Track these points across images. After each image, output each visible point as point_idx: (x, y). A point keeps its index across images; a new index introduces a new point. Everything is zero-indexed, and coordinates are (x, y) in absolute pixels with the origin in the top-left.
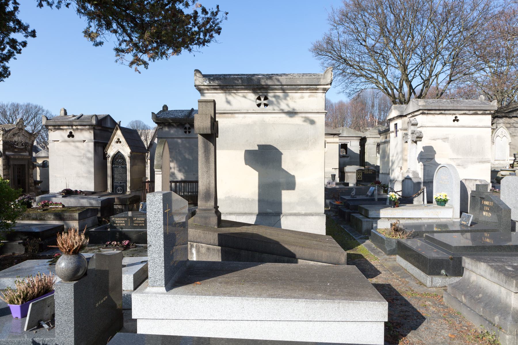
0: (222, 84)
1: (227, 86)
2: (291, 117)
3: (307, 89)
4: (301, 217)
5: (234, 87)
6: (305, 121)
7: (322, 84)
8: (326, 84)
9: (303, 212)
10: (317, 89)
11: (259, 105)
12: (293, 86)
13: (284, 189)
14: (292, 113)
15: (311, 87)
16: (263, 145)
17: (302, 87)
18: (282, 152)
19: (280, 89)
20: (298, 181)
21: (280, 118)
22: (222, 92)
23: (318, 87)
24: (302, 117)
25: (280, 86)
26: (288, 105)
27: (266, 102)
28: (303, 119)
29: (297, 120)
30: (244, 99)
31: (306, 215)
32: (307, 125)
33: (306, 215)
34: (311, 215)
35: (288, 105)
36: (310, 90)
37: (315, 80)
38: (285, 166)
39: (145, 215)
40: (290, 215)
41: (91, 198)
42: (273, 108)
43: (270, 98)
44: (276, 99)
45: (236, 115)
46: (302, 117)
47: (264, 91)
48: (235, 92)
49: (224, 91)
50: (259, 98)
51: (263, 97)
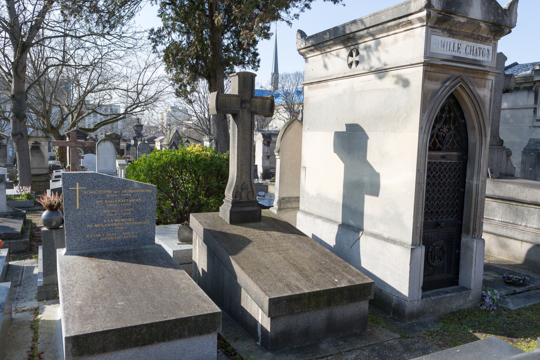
0: (315, 43)
1: (319, 44)
2: (381, 78)
3: (398, 26)
4: (380, 241)
5: (325, 44)
6: (396, 83)
7: (412, 11)
8: (417, 10)
9: (386, 235)
10: (410, 23)
11: (350, 65)
12: (380, 27)
13: (367, 194)
14: (381, 72)
15: (401, 20)
16: (350, 124)
17: (389, 24)
18: (369, 135)
19: (368, 35)
20: (383, 182)
21: (369, 81)
22: (319, 53)
23: (410, 18)
24: (393, 76)
25: (366, 31)
26: (379, 59)
27: (357, 59)
28: (394, 79)
29: (389, 81)
30: (337, 58)
31: (388, 240)
32: (399, 88)
33: (388, 240)
34: (394, 242)
35: (379, 59)
36: (403, 26)
37: (404, 6)
38: (370, 158)
39: (244, 198)
40: (370, 236)
41: (515, 183)
42: (364, 67)
43: (361, 52)
44: (367, 52)
45: (330, 83)
46: (393, 76)
47: (354, 42)
48: (329, 50)
49: (320, 51)
50: (351, 55)
51: (354, 51)
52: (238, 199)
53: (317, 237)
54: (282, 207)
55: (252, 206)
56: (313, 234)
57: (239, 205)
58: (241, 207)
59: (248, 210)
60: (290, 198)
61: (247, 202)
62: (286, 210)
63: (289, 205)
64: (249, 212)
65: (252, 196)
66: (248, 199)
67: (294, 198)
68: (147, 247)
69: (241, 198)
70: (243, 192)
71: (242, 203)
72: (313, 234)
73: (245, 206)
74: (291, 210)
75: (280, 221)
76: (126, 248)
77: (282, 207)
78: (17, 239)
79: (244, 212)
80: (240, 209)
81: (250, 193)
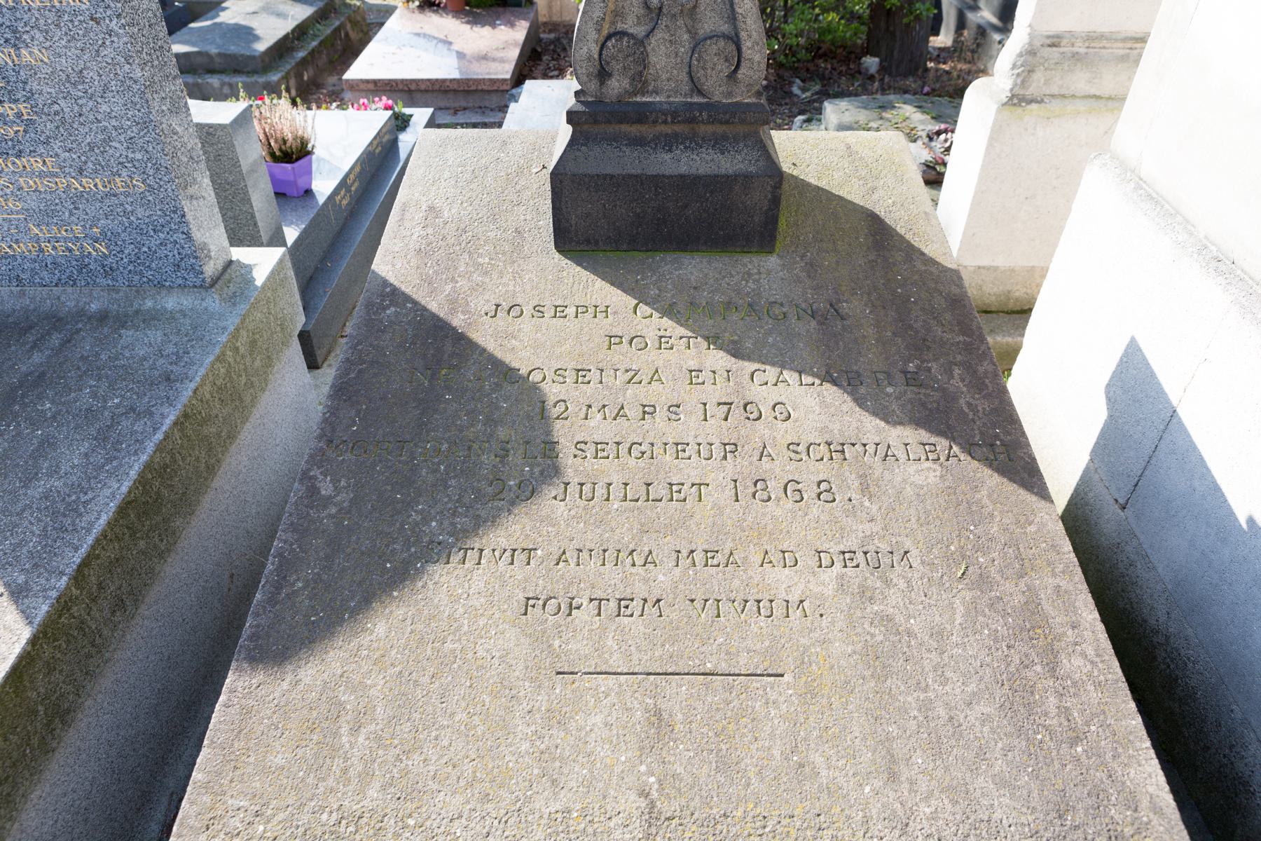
52: (617, 85)
53: (1152, 375)
54: (1037, 85)
55: (718, 143)
56: (1133, 340)
57: (625, 128)
58: (638, 142)
59: (683, 169)
60: (1102, 37)
61: (686, 115)
62: (1055, 105)
63: (1079, 81)
64: (688, 183)
65: (725, 69)
66: (697, 89)
67: (1125, 40)
68: (171, 302)
69: (640, 81)
70: (659, 34)
71: (642, 115)
72: (1133, 340)
73: (669, 142)
74: (1081, 106)
75: (911, 252)
76: (70, 299)
77: (1033, 90)
78: (255, 72)
79: (656, 180)
80: (629, 162)
81: (712, 48)
